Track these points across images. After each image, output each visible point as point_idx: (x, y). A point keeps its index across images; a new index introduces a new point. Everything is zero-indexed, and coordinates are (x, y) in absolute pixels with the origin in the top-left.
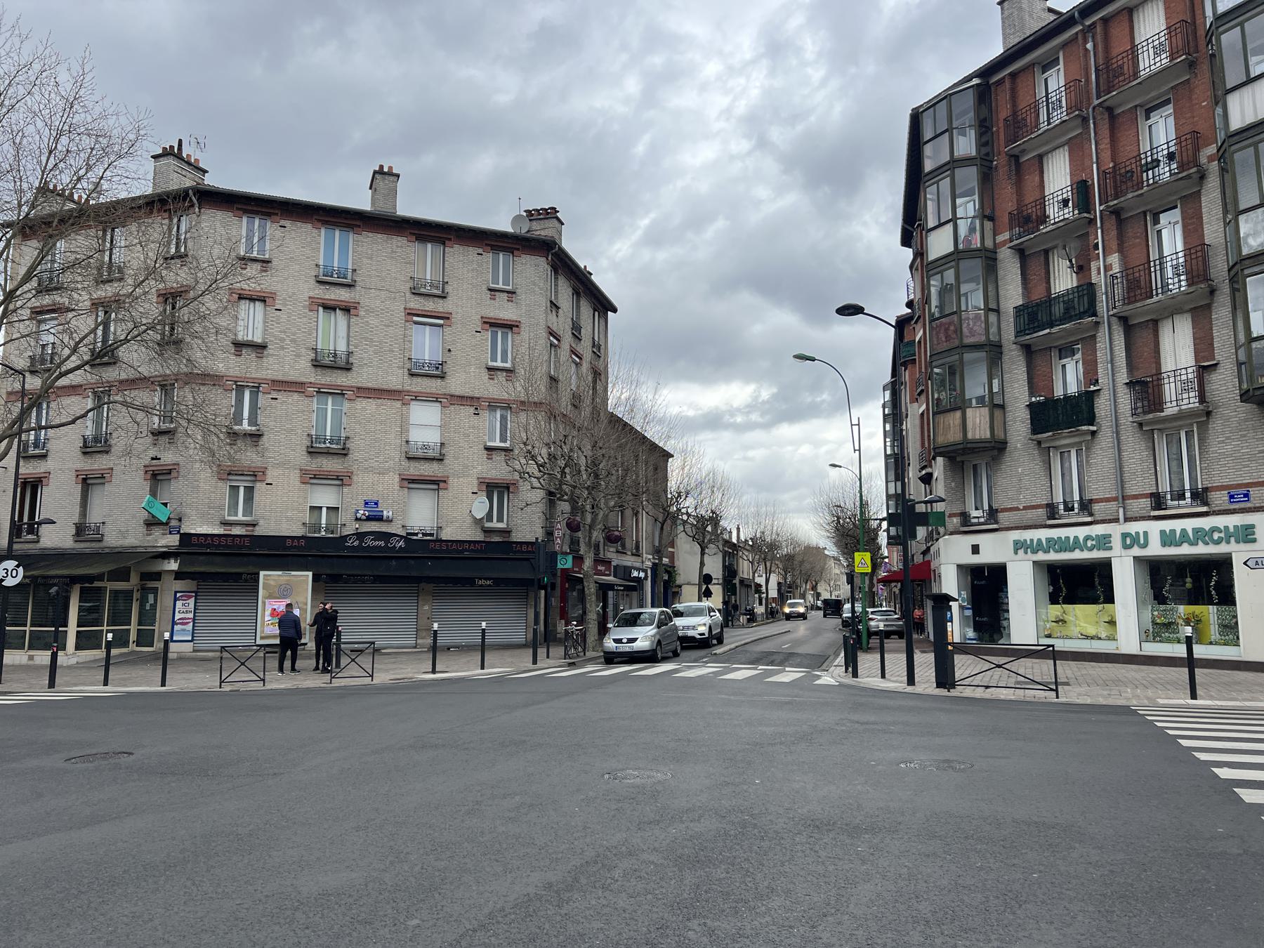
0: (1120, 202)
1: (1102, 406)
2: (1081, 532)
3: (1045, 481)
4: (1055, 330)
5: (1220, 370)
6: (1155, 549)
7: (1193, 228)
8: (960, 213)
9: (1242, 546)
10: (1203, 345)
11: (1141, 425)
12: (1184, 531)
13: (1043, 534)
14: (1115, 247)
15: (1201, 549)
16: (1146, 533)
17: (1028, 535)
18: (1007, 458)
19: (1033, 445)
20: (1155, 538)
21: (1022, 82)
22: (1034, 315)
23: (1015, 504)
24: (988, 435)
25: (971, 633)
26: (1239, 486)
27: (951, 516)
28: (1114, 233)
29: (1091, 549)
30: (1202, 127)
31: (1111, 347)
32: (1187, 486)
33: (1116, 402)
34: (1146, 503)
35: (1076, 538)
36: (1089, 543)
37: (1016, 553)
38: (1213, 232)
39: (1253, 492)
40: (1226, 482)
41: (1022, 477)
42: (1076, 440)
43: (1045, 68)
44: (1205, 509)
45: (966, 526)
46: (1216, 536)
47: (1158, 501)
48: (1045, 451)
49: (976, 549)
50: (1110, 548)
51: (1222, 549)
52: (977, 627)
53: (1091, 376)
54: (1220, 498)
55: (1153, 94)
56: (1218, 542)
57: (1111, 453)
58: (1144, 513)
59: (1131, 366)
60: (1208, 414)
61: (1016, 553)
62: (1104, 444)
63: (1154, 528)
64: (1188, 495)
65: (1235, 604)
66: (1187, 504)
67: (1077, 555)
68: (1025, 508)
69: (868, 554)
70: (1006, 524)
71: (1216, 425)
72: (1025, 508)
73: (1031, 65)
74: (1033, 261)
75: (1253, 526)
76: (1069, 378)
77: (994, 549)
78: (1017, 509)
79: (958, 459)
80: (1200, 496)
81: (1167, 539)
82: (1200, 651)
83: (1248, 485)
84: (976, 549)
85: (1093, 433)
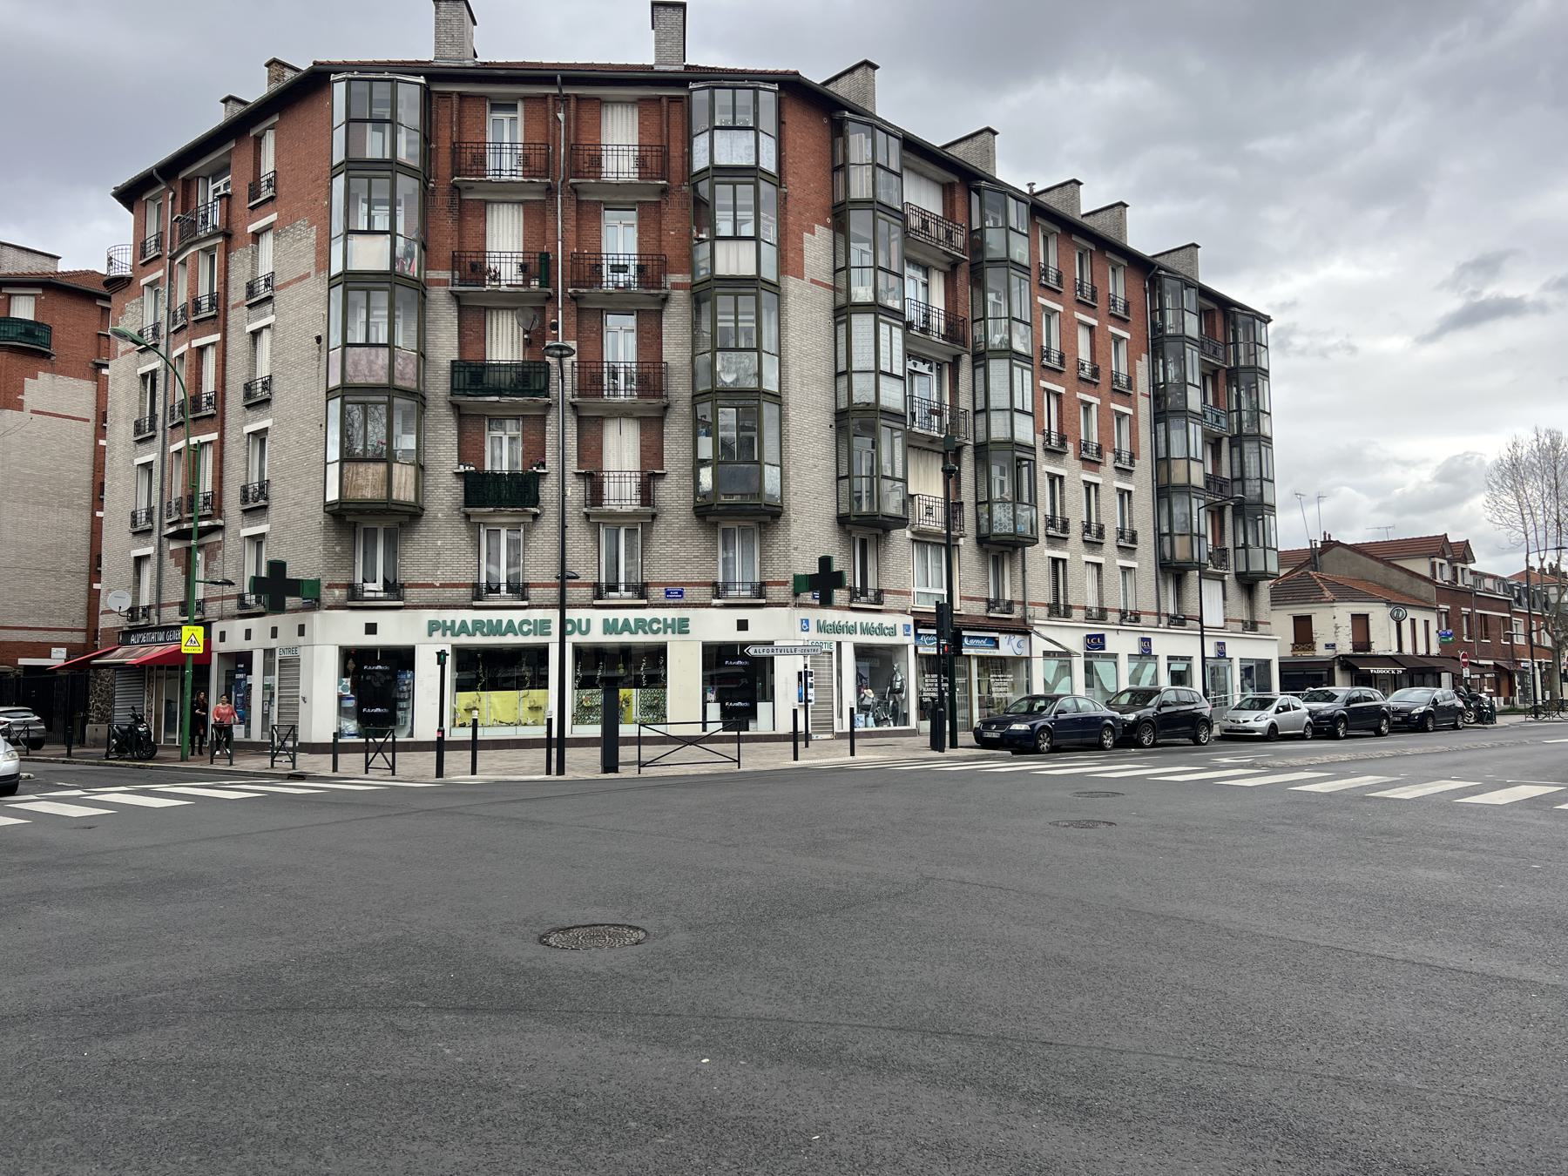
0: (563, 289)
1: (548, 490)
2: (517, 616)
3: (471, 558)
4: (505, 399)
5: (667, 479)
6: (597, 636)
7: (650, 339)
8: (854, 261)
9: (677, 636)
10: (652, 455)
11: (587, 516)
12: (464, 623)
13: (469, 616)
14: (574, 334)
15: (641, 638)
16: (588, 621)
17: (448, 616)
18: (422, 527)
19: (458, 517)
20: (718, 626)
21: (470, 109)
22: (472, 375)
23: (429, 580)
24: (412, 499)
25: (351, 726)
26: (675, 584)
27: (330, 586)
28: (574, 319)
29: (526, 634)
30: (671, 252)
31: (561, 434)
32: (622, 579)
33: (560, 487)
34: (589, 591)
35: (510, 622)
36: (525, 628)
37: (430, 635)
38: (674, 351)
39: (686, 590)
40: (663, 579)
41: (440, 551)
42: (515, 520)
43: (496, 107)
44: (525, 603)
45: (354, 599)
46: (655, 627)
47: (599, 591)
48: (474, 528)
49: (371, 629)
50: (549, 634)
51: (660, 638)
52: (362, 719)
53: (535, 452)
54: (657, 593)
55: (620, 199)
56: (656, 632)
57: (556, 539)
58: (584, 601)
59: (580, 459)
60: (654, 516)
61: (430, 635)
62: (546, 529)
63: (597, 617)
64: (503, 588)
65: (665, 687)
66: (624, 596)
67: (510, 639)
68: (442, 586)
69: (201, 629)
70: (415, 602)
71: (659, 528)
72: (442, 586)
73: (483, 97)
74: (474, 313)
75: (1366, 616)
76: (502, 453)
77: (395, 629)
78: (432, 586)
79: (348, 519)
80: (641, 590)
81: (609, 627)
82: (482, 734)
83: (683, 584)
84: (371, 629)
85: (536, 516)
